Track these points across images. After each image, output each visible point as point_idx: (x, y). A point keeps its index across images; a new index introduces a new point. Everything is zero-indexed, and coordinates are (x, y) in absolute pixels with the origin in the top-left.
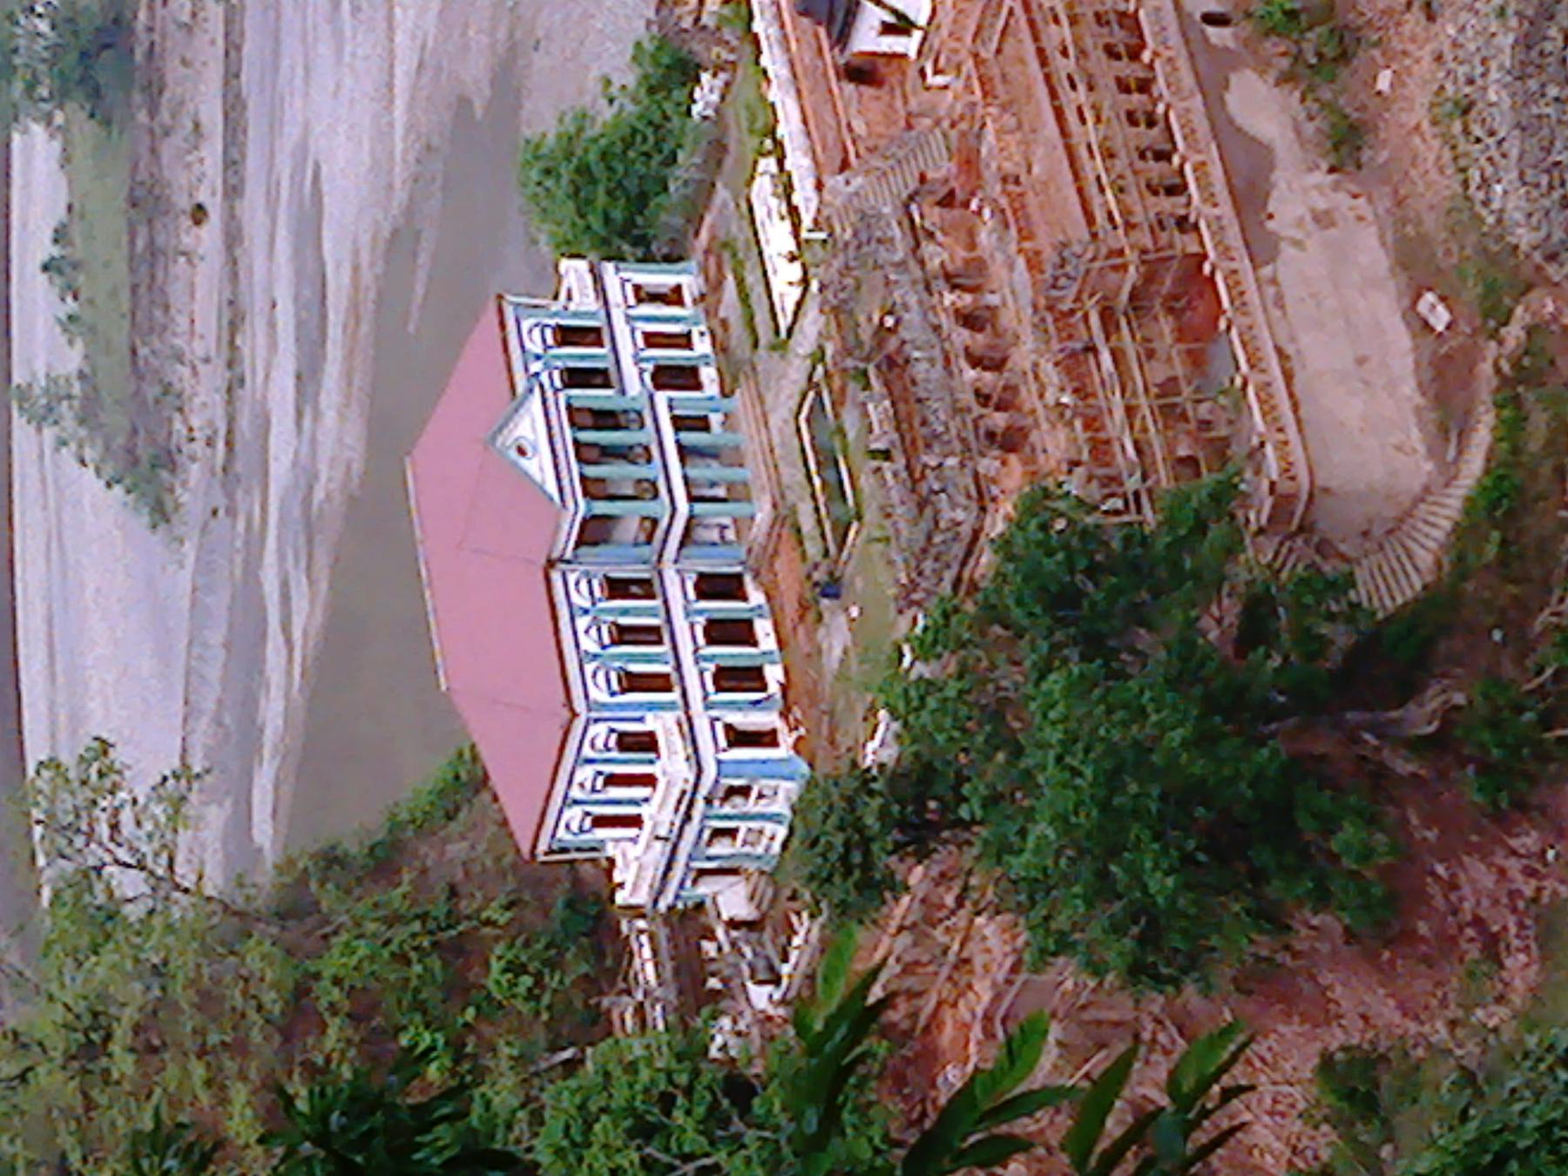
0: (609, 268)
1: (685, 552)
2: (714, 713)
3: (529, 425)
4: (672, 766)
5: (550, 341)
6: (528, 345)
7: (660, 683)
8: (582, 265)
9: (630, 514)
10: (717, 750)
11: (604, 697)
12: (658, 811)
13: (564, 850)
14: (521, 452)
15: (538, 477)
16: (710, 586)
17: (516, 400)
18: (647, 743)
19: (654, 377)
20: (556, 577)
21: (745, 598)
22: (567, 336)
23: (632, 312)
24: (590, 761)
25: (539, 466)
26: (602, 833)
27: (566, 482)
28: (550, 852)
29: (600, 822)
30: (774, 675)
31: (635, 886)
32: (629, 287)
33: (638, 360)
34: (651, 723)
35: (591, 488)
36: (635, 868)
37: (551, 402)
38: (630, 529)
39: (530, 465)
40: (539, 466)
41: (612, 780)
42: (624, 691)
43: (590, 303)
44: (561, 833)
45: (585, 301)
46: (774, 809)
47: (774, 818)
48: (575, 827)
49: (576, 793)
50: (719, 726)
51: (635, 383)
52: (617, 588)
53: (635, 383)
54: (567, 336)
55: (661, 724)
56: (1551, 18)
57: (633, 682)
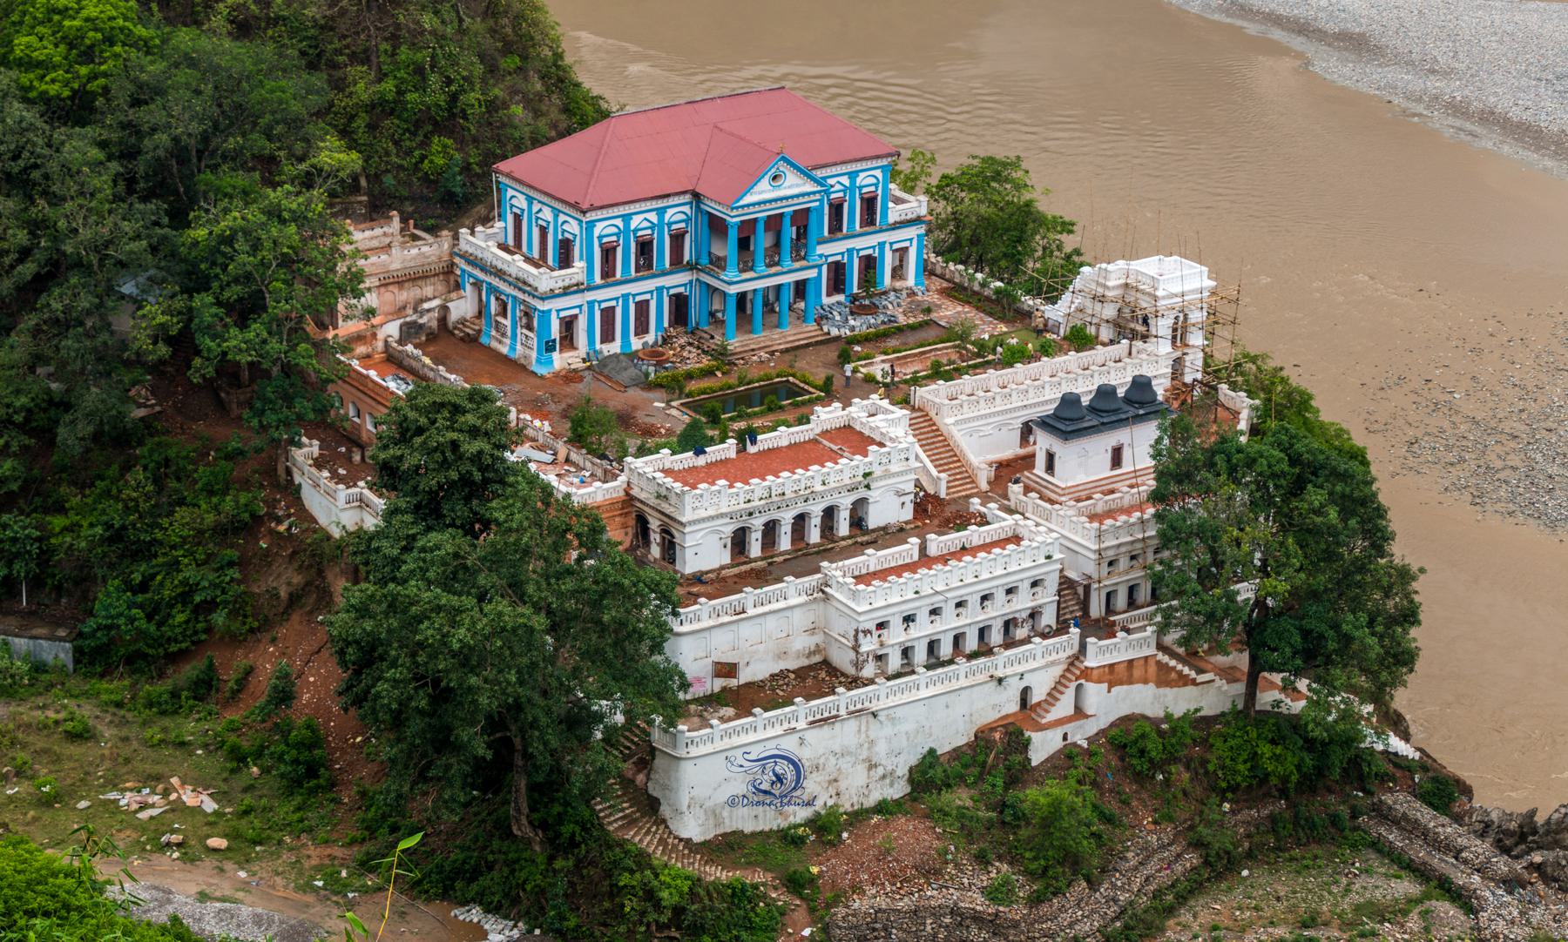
0: (922, 230)
1: (704, 288)
2: (585, 308)
3: (794, 185)
4: (545, 280)
5: (865, 190)
6: (862, 175)
7: (608, 272)
8: (923, 211)
9: (729, 250)
10: (558, 311)
11: (597, 232)
12: (516, 265)
13: (499, 190)
14: (775, 178)
15: (757, 189)
16: (680, 305)
17: (806, 173)
18: (565, 261)
19: (837, 263)
20: (687, 198)
21: (829, 295)
22: (869, 203)
23: (887, 247)
24: (556, 221)
25: (763, 191)
26: (510, 218)
27: (752, 209)
28: (498, 182)
29: (518, 219)
30: (615, 347)
31: (468, 242)
32: (906, 244)
33: (850, 251)
34: (579, 265)
35: (748, 227)
36: (482, 241)
37: (812, 197)
38: (718, 250)
39: (765, 184)
40: (763, 191)
41: (543, 231)
42: (601, 245)
43: (893, 217)
44: (511, 192)
45: (895, 213)
46: (519, 347)
47: (513, 348)
48: (514, 202)
49: (536, 207)
50: (576, 311)
51: (834, 250)
52: (677, 239)
53: (834, 250)
54: (869, 203)
55: (578, 269)
56: (995, 934)
57: (608, 253)
